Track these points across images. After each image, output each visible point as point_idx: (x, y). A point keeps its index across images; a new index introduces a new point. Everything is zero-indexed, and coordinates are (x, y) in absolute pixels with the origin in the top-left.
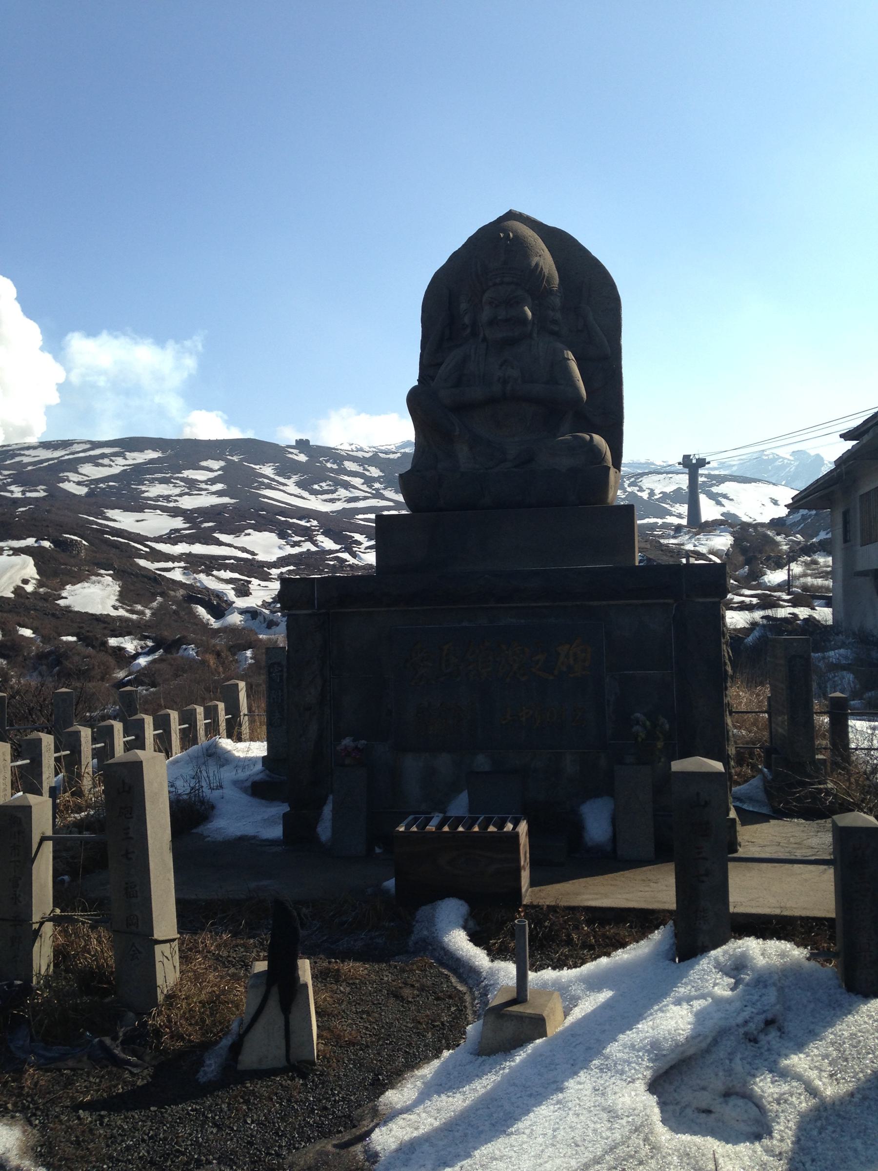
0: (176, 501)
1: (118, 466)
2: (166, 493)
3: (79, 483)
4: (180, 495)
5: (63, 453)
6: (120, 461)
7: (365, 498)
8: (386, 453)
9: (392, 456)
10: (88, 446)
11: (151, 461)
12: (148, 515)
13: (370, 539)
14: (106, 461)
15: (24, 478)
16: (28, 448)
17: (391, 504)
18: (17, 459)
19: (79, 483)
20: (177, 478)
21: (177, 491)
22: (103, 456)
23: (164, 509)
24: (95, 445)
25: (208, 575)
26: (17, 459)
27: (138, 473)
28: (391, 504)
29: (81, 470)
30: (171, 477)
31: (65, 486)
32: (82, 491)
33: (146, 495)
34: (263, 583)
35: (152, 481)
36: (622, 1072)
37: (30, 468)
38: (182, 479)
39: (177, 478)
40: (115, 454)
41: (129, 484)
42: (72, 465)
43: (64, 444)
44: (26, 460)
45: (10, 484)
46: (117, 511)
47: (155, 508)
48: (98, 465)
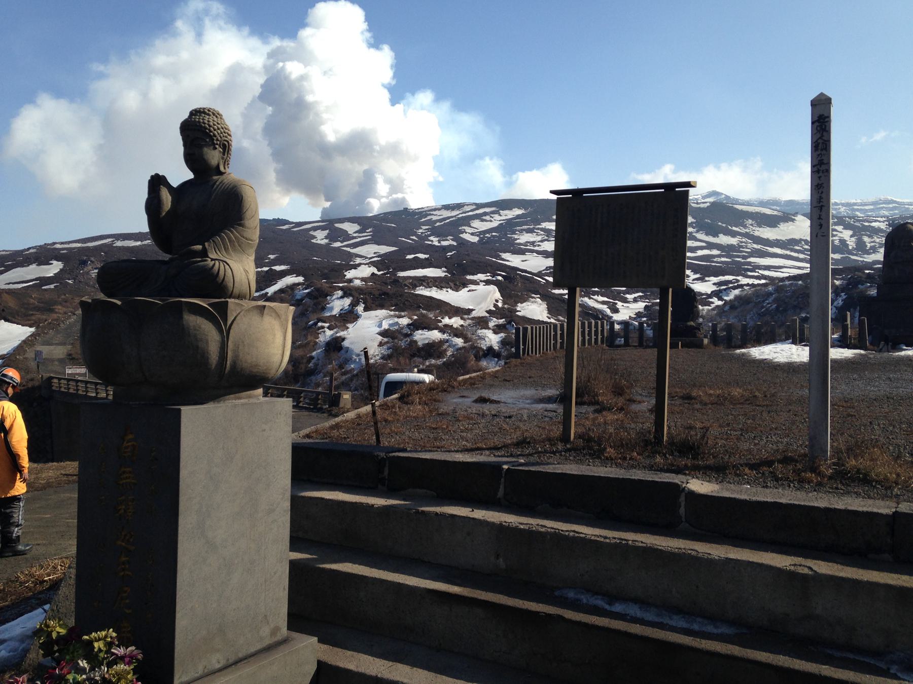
0: (539, 245)
1: (496, 221)
2: (532, 240)
3: (472, 234)
4: (542, 241)
5: (458, 212)
6: (496, 217)
7: (702, 248)
8: (697, 203)
9: (702, 206)
10: (474, 207)
11: (518, 217)
12: (528, 256)
13: (695, 273)
14: (488, 218)
15: (440, 232)
16: (435, 210)
17: (704, 244)
18: (429, 218)
19: (472, 234)
20: (538, 229)
21: (539, 238)
22: (485, 214)
23: (539, 253)
24: (479, 206)
25: (590, 298)
26: (429, 218)
27: (509, 226)
28: (704, 244)
29: (472, 225)
30: (534, 228)
31: (464, 236)
32: (475, 239)
33: (518, 241)
34: (625, 305)
35: (521, 231)
36: (875, 487)
37: (438, 224)
38: (542, 229)
39: (538, 229)
40: (493, 212)
41: (506, 234)
42: (467, 221)
43: (459, 206)
44: (434, 218)
45: (430, 236)
46: (508, 254)
47: (532, 251)
48: (483, 220)
